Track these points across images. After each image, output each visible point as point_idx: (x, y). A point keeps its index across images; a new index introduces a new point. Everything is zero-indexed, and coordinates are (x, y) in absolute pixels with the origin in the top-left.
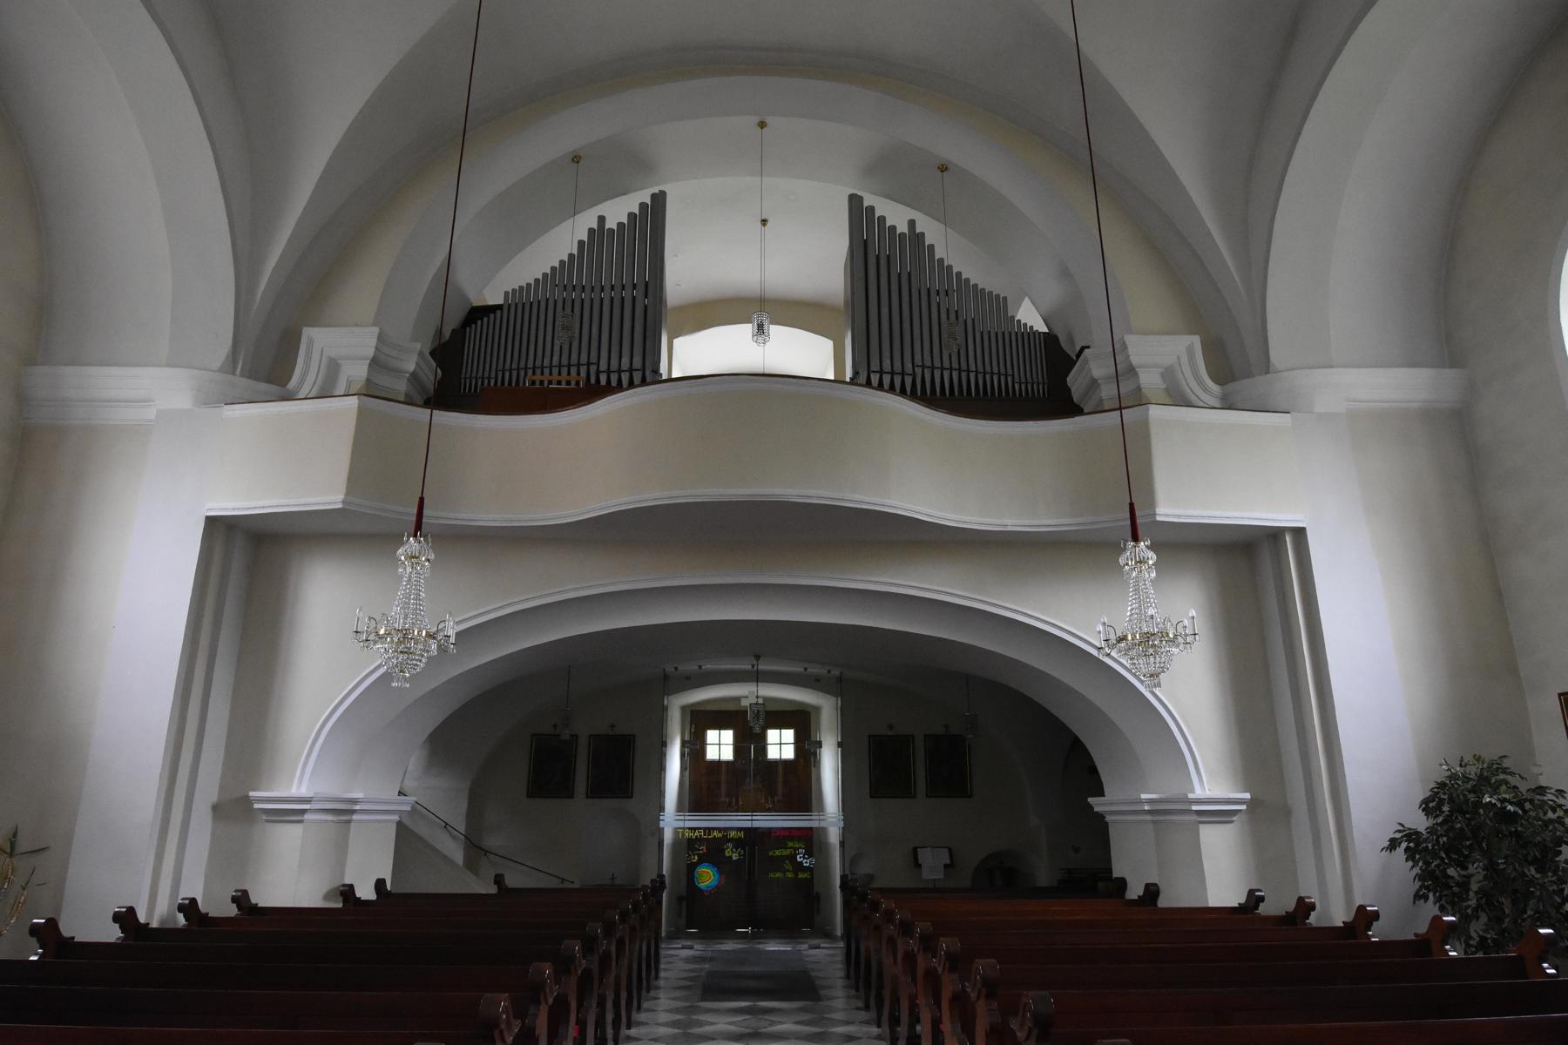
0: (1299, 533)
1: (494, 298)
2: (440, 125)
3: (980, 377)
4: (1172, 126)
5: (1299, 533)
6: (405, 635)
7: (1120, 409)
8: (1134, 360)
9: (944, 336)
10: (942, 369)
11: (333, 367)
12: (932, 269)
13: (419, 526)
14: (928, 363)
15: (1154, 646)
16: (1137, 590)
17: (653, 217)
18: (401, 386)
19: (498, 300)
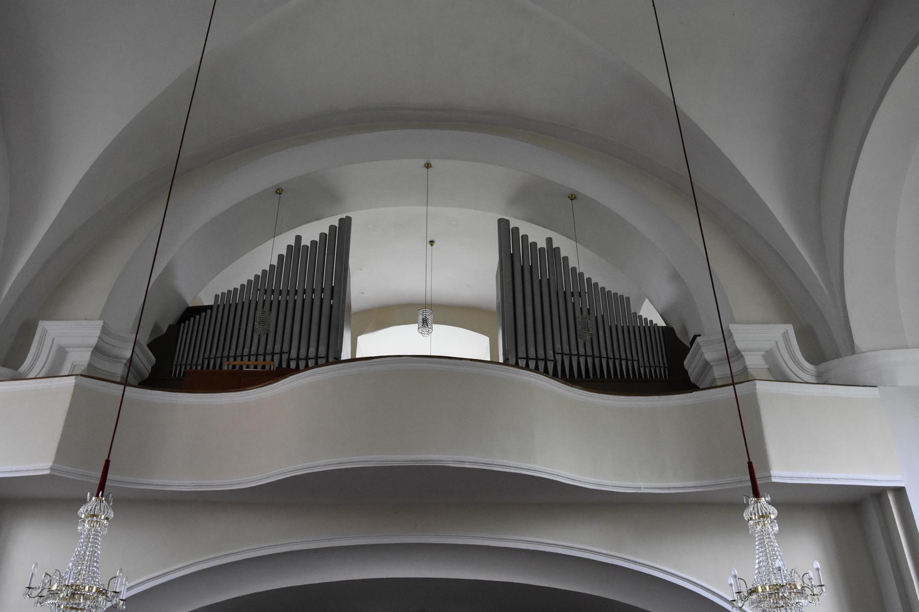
0: (900, 492)
1: (207, 300)
2: (168, 164)
3: (611, 362)
4: (752, 157)
5: (900, 492)
6: (75, 592)
7: (733, 384)
8: (740, 345)
9: (579, 328)
10: (578, 355)
11: (61, 353)
12: (567, 273)
13: (102, 487)
14: (566, 351)
15: (783, 598)
16: (762, 543)
17: (339, 239)
18: (119, 370)
19: (208, 301)
